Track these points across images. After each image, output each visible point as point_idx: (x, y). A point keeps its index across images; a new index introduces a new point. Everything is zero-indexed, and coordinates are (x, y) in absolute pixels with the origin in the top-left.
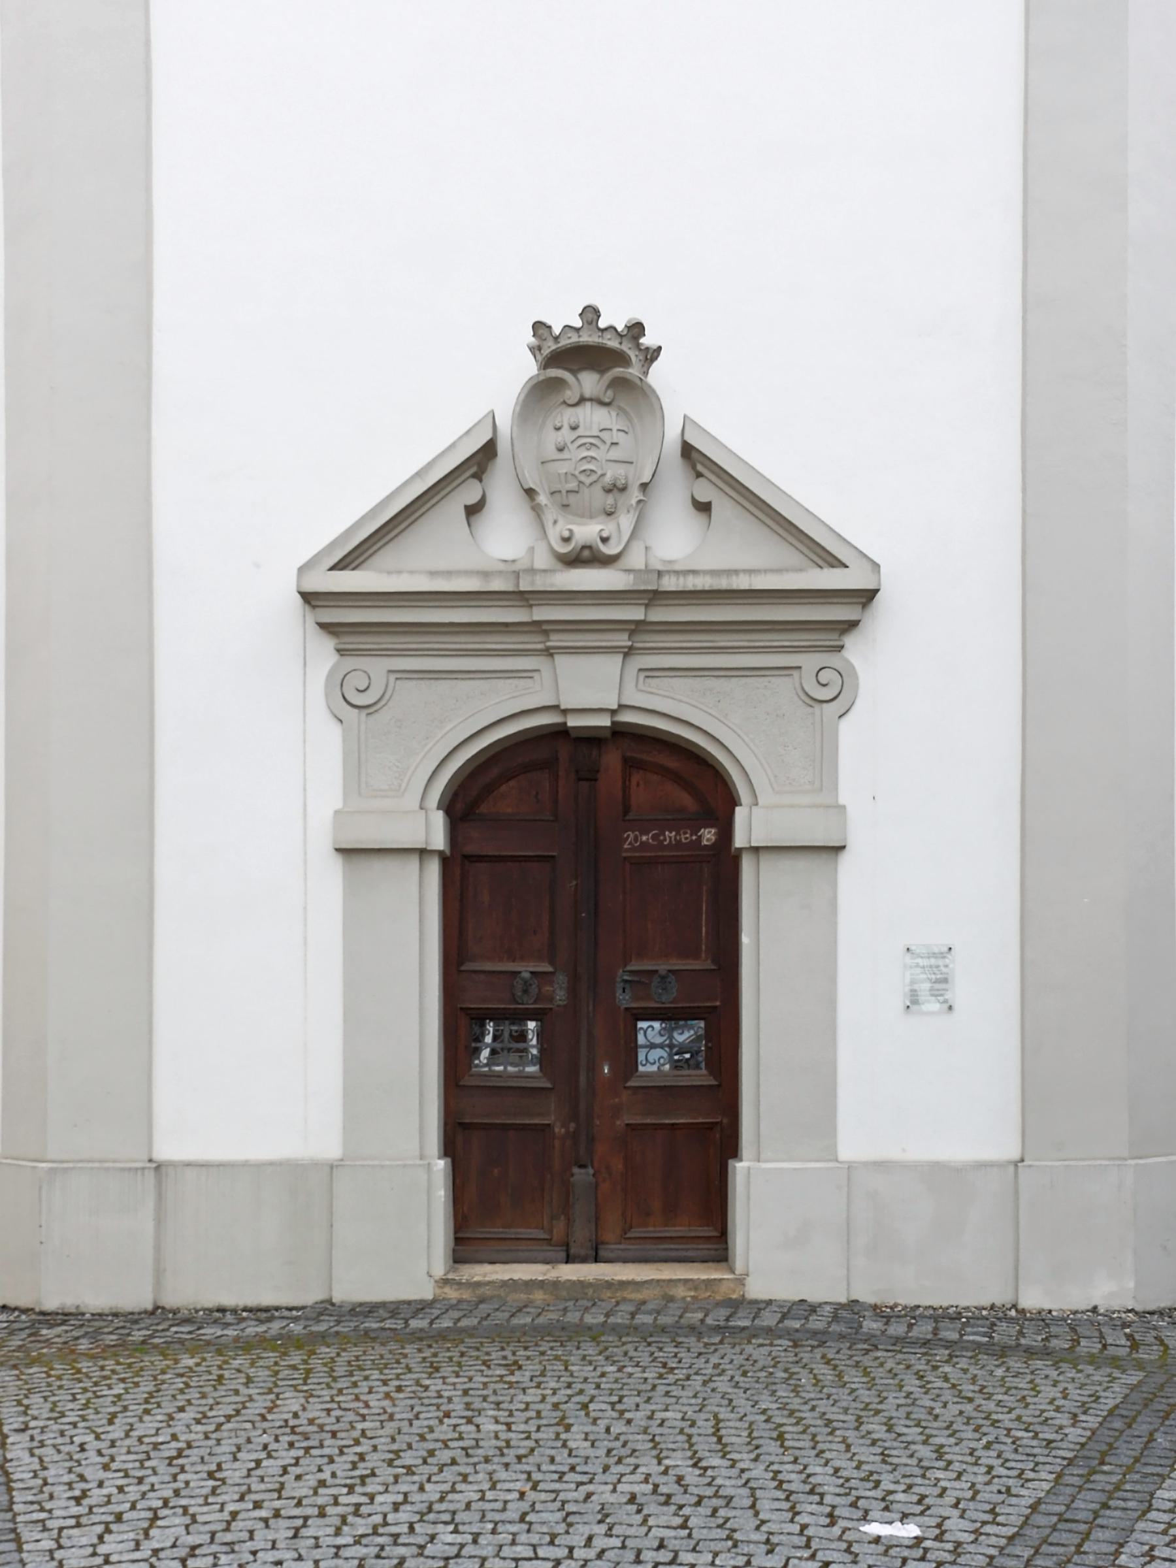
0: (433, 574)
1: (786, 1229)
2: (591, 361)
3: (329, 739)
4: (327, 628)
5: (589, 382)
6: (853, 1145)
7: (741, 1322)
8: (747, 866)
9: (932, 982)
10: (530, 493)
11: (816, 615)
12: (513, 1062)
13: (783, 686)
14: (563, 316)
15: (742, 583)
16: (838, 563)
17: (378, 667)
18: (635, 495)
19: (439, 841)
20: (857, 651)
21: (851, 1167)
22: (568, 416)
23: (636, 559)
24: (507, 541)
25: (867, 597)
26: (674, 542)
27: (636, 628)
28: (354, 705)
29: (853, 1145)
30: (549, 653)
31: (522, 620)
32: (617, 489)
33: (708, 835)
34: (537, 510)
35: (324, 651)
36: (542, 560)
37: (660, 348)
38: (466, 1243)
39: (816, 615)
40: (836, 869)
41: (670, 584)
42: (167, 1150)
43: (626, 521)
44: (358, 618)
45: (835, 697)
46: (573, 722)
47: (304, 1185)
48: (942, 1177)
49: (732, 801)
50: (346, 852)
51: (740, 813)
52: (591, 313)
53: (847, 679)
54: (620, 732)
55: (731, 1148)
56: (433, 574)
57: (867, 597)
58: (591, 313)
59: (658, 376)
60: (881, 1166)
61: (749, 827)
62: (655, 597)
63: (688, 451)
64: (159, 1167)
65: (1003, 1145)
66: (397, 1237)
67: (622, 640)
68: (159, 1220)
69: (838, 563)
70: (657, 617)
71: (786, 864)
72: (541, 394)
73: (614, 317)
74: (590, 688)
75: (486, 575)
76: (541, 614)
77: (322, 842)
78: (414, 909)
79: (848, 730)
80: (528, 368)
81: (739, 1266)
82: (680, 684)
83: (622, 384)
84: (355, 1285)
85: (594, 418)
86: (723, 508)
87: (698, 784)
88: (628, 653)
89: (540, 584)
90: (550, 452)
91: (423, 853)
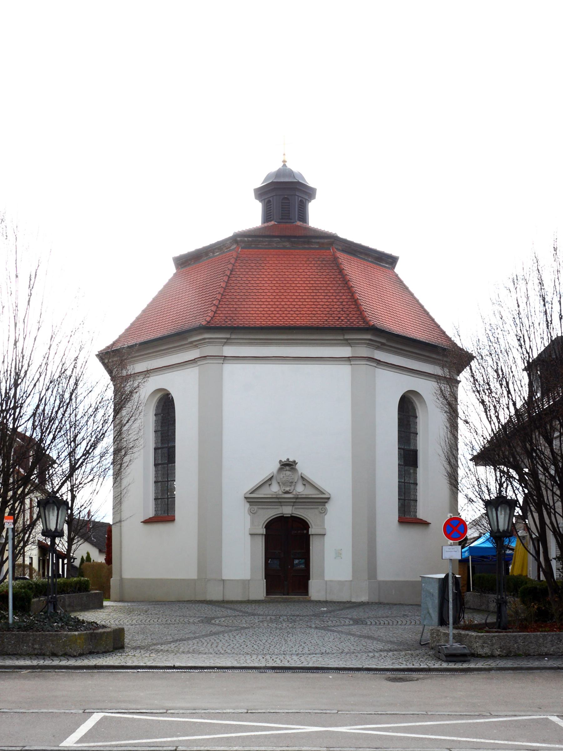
0: (264, 494)
1: (316, 590)
2: (288, 466)
3: (248, 518)
4: (248, 502)
5: (288, 468)
6: (327, 578)
7: (119, 522)
8: (311, 537)
9: (338, 554)
10: (279, 483)
11: (321, 501)
12: (276, 564)
13: (316, 510)
14: (284, 459)
15: (310, 496)
16: (324, 494)
17: (256, 507)
18: (294, 484)
19: (265, 533)
20: (327, 506)
21: (326, 581)
22: (284, 472)
23: (294, 493)
24: (275, 489)
25: (329, 498)
26: (300, 489)
27: (294, 502)
28: (252, 513)
29: (327, 578)
30: (281, 505)
31: (277, 501)
32: (292, 483)
33: (305, 532)
34: (280, 485)
35: (248, 505)
36: (280, 493)
37: (285, 196)
38: (268, 593)
39: (321, 501)
40: (324, 539)
41: (299, 496)
42: (224, 578)
43: (293, 487)
44: (253, 501)
45: (325, 512)
46: (285, 516)
47: (245, 583)
48: (341, 583)
49: (309, 527)
50: (251, 534)
51: (310, 529)
52: (288, 459)
53: (326, 509)
54: (292, 516)
55: (309, 578)
56: (264, 494)
57: (329, 498)
58: (288, 459)
59: (297, 467)
60: (331, 581)
61: (311, 531)
62: (297, 498)
63: (302, 477)
64: (223, 580)
65: (350, 578)
66: (259, 590)
67: (292, 504)
68: (223, 588)
69: (324, 494)
70: (298, 501)
71: (317, 536)
72: (280, 470)
73: (291, 460)
74: (287, 511)
75: (272, 495)
76: (280, 500)
77: (247, 533)
78: (260, 544)
79: (326, 517)
80: (278, 466)
81: (310, 595)
82: (301, 510)
83: (293, 468)
84: (252, 597)
85: (288, 473)
86: (307, 485)
87: (303, 525)
88: (293, 506)
89: (280, 496)
90: (282, 477)
91: (262, 535)
